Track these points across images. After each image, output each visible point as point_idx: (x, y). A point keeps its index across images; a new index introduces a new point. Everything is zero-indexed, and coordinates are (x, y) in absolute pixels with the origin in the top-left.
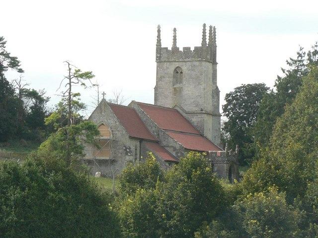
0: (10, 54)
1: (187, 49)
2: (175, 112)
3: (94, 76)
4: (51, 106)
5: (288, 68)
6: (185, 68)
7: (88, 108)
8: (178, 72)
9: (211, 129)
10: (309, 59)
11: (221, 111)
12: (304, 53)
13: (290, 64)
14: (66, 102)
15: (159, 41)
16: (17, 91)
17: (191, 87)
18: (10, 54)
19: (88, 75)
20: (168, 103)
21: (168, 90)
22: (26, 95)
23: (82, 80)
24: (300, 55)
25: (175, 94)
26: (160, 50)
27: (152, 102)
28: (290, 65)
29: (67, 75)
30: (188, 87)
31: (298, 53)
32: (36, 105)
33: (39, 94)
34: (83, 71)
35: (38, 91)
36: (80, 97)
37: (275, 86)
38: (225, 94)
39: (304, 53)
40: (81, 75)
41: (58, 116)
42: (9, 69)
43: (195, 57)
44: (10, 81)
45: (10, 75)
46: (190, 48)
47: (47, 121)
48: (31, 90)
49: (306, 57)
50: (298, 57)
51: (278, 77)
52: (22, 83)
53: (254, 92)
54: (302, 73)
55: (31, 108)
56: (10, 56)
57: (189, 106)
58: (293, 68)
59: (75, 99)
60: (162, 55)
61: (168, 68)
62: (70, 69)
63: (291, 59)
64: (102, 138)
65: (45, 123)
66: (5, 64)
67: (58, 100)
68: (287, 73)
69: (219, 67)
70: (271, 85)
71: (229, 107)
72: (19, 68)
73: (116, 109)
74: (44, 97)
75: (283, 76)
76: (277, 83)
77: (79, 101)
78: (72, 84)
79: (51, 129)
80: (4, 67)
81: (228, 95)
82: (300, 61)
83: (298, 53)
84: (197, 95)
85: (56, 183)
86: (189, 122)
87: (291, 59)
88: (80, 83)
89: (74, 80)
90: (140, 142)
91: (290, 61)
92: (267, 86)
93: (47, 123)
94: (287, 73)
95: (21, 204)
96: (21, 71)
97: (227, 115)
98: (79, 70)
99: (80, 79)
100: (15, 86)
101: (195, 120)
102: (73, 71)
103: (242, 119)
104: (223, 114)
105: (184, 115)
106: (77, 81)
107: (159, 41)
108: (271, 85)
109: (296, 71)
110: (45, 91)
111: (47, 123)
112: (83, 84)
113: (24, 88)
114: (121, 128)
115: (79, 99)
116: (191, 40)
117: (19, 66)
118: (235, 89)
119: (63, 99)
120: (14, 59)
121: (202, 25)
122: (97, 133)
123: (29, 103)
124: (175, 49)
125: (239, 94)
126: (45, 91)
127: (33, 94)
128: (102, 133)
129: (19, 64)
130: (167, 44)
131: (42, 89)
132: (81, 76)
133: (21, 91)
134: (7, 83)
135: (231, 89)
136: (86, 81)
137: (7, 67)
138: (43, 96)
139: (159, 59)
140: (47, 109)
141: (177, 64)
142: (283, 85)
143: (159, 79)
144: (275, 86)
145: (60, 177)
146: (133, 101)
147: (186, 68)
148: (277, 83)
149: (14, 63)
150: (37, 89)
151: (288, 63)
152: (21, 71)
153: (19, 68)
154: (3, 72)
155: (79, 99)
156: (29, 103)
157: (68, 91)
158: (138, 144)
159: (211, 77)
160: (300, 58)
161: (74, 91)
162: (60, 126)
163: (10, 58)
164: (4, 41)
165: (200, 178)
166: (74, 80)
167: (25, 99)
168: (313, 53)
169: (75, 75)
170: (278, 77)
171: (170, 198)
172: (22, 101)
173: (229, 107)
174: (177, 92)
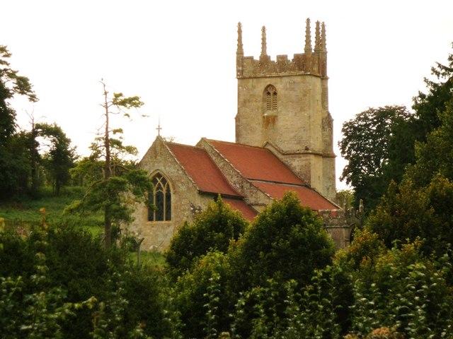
1: (282, 59)
2: (266, 154)
6: (280, 86)
8: (270, 91)
13: (438, 74)
15: (240, 46)
19: (133, 102)
20: (256, 139)
26: (242, 60)
27: (230, 138)
34: (126, 96)
56: (18, 75)
58: (444, 80)
61: (254, 87)
62: (106, 93)
73: (180, 151)
77: (121, 140)
84: (299, 125)
86: (287, 168)
87: (440, 66)
91: (438, 69)
98: (121, 95)
101: (296, 164)
102: (111, 97)
105: (280, 156)
107: (240, 46)
115: (121, 138)
116: (288, 45)
123: (45, 146)
124: (265, 59)
127: (54, 132)
132: (123, 103)
135: (351, 116)
136: (132, 110)
139: (242, 77)
141: (268, 81)
143: (243, 103)
149: (23, 85)
152: (33, 98)
161: (112, 127)
166: (113, 108)
167: (38, 139)
174: (270, 121)
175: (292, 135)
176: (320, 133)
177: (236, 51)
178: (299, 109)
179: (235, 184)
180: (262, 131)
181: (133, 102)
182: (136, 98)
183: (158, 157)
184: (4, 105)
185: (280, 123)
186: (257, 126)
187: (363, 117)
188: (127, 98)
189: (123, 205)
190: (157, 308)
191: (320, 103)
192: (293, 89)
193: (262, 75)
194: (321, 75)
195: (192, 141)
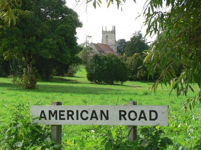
1: (109, 31)
2: (106, 46)
6: (109, 35)
8: (107, 36)
15: (103, 29)
19: (90, 37)
20: (105, 43)
21: (105, 40)
26: (103, 31)
27: (101, 43)
46: (76, 35)
53: (122, 41)
57: (109, 44)
58: (134, 35)
59: (88, 42)
60: (104, 32)
69: (116, 35)
73: (95, 44)
75: (132, 37)
85: (114, 60)
86: (110, 48)
89: (87, 38)
95: (107, 64)
101: (111, 47)
103: (120, 47)
105: (109, 46)
107: (103, 29)
114: (96, 49)
116: (110, 29)
124: (106, 31)
130: (104, 30)
136: (90, 38)
139: (103, 33)
143: (103, 38)
145: (115, 59)
146: (123, 40)
149: (78, 38)
161: (87, 40)
165: (138, 59)
166: (87, 38)
171: (131, 64)
174: (107, 41)
177: (147, 28)
181: (90, 37)
184: (75, 29)
189: (85, 46)
195: (96, 43)
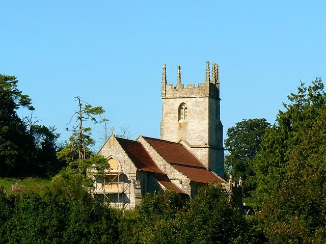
0: (21, 92)
3: (104, 111)
4: (63, 140)
5: (289, 102)
7: (97, 143)
9: (215, 163)
10: (309, 94)
11: (224, 146)
12: (305, 89)
13: (292, 100)
14: (77, 137)
16: (29, 128)
17: (196, 122)
18: (21, 92)
19: (99, 110)
22: (36, 132)
23: (92, 115)
24: (301, 90)
25: (180, 129)
28: (291, 100)
29: (78, 110)
30: (192, 122)
31: (299, 89)
32: (46, 141)
33: (50, 131)
34: (94, 106)
35: (48, 128)
36: (91, 132)
37: (277, 120)
38: (227, 129)
39: (305, 89)
40: (92, 110)
41: (69, 151)
42: (21, 107)
43: (199, 94)
44: (22, 118)
45: (21, 112)
47: (59, 156)
48: (42, 127)
49: (307, 92)
50: (299, 92)
51: (280, 112)
52: (34, 120)
53: (259, 125)
54: (303, 108)
55: (42, 144)
56: (22, 94)
58: (295, 103)
59: (86, 134)
61: (173, 104)
62: (81, 105)
63: (292, 94)
64: (111, 171)
65: (57, 157)
66: (17, 102)
67: (70, 134)
68: (289, 108)
70: (272, 120)
71: (231, 142)
72: (30, 105)
74: (55, 133)
75: (285, 110)
76: (279, 117)
77: (89, 135)
78: (82, 119)
79: (62, 164)
80: (16, 105)
81: (230, 130)
82: (300, 96)
83: (299, 89)
84: (202, 129)
87: (292, 94)
88: (90, 118)
90: (148, 176)
91: (291, 96)
92: (268, 121)
93: (58, 158)
94: (289, 108)
96: (32, 108)
97: (230, 150)
98: (90, 106)
99: (90, 114)
100: (27, 122)
102: (83, 107)
104: (226, 148)
106: (87, 116)
108: (272, 120)
109: (298, 106)
110: (55, 128)
111: (58, 158)
112: (94, 119)
113: (35, 125)
114: (129, 161)
115: (90, 134)
117: (30, 104)
118: (237, 124)
119: (74, 134)
120: (25, 97)
121: (108, 119)
122: (108, 167)
123: (40, 139)
125: (240, 129)
126: (55, 128)
127: (44, 131)
128: (112, 166)
129: (30, 102)
131: (52, 126)
132: (92, 111)
133: (32, 128)
134: (19, 120)
135: (233, 125)
136: (97, 117)
137: (19, 105)
138: (54, 132)
140: (57, 145)
141: (182, 101)
142: (285, 120)
144: (277, 120)
147: (190, 104)
148: (279, 117)
149: (25, 102)
150: (48, 126)
151: (289, 98)
152: (32, 108)
153: (30, 105)
154: (15, 110)
155: (90, 134)
156: (40, 139)
157: (79, 126)
158: (146, 177)
159: (215, 112)
160: (300, 94)
161: (84, 126)
162: (71, 161)
163: (22, 96)
164: (16, 80)
166: (85, 115)
167: (35, 136)
168: (313, 88)
169: (86, 111)
170: (280, 112)
172: (34, 138)
173: (231, 142)
175: (197, 135)
176: (215, 134)
178: (201, 118)
179: (160, 166)
180: (178, 132)
182: (100, 108)
183: (112, 148)
185: (189, 127)
186: (174, 129)
187: (240, 125)
188: (94, 108)
190: (209, 97)
191: (215, 115)
192: (198, 106)
193: (178, 96)
194: (215, 97)
